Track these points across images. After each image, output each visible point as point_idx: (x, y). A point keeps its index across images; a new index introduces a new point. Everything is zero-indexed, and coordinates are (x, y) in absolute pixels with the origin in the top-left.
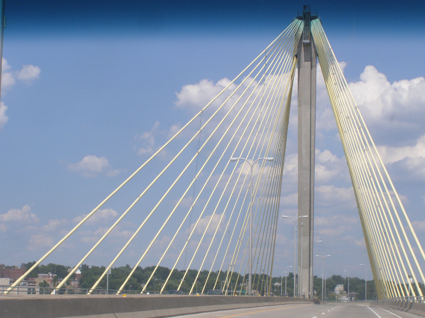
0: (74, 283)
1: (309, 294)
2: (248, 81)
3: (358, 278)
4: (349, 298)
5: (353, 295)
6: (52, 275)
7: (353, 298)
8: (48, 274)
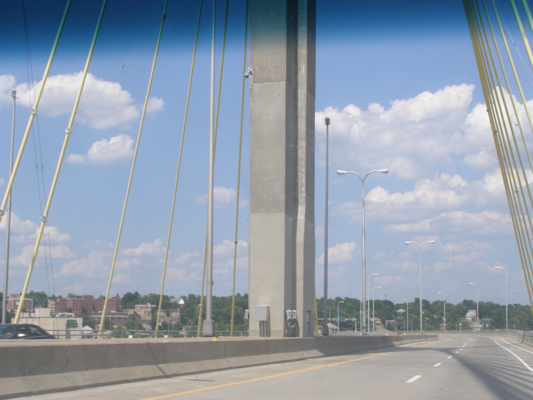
0: (176, 315)
1: (286, 317)
2: (375, 107)
3: (492, 303)
4: (482, 325)
5: (487, 321)
6: (151, 306)
7: (487, 325)
8: (147, 304)
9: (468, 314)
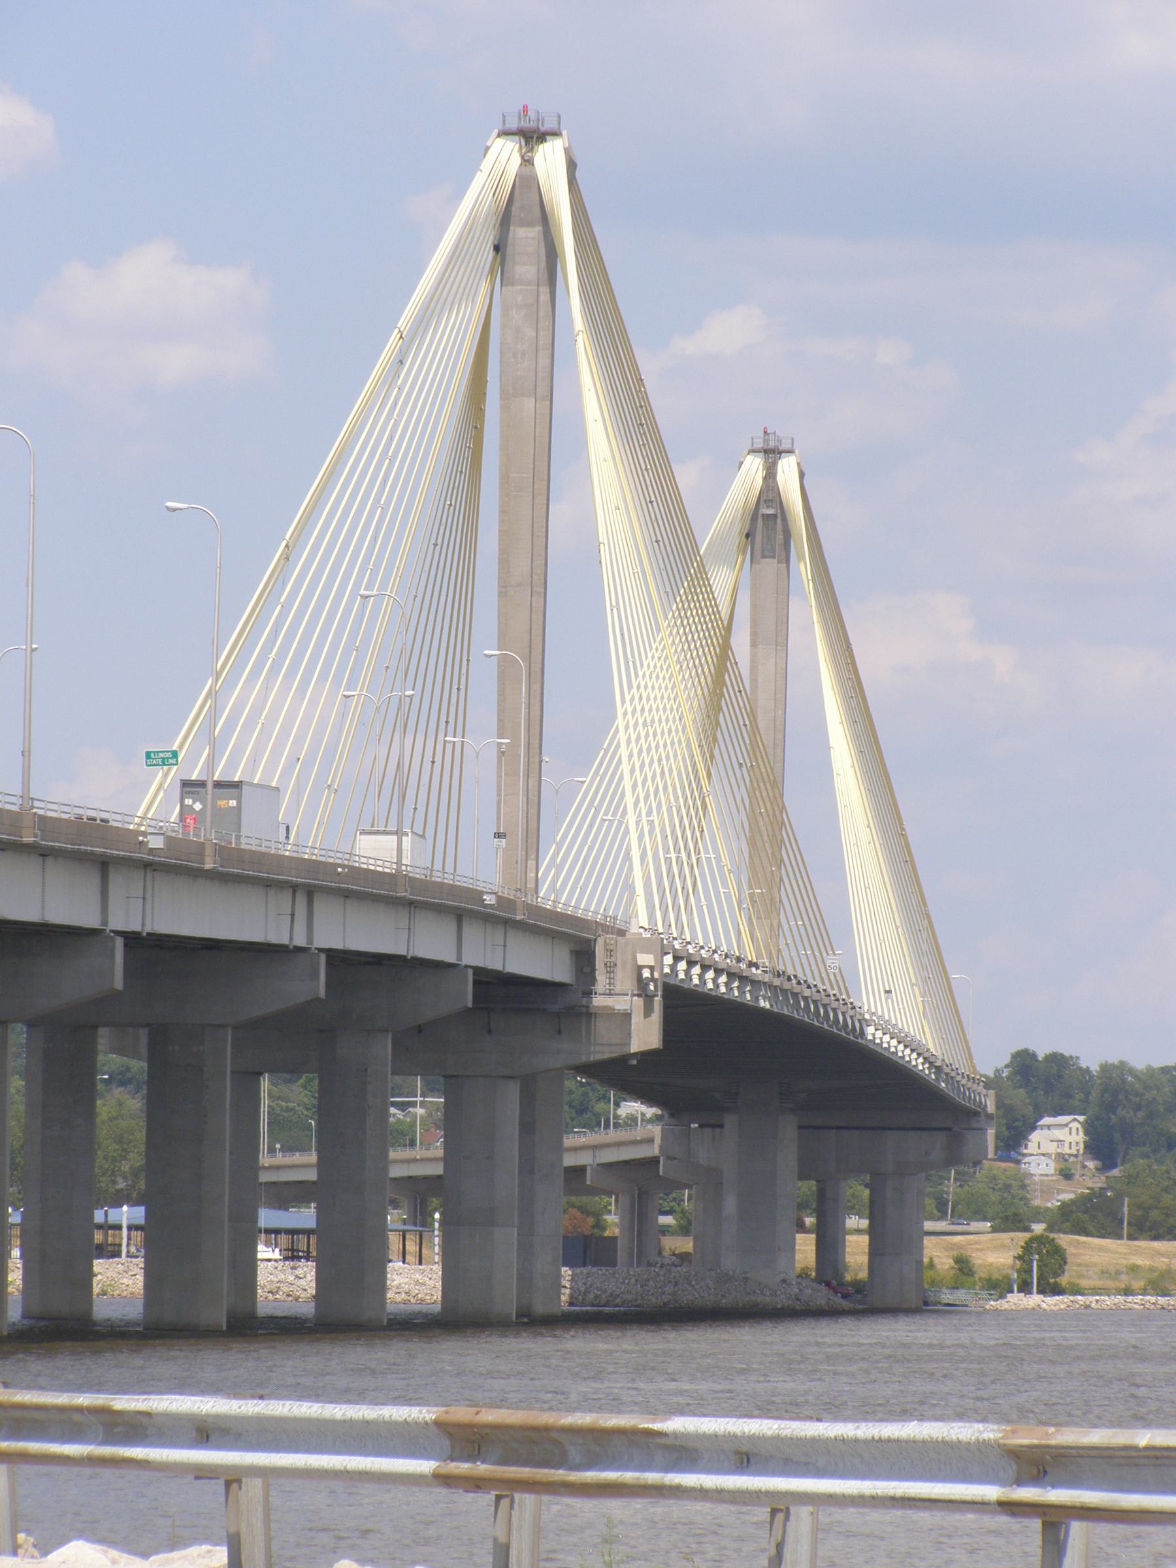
9: (1035, 1137)
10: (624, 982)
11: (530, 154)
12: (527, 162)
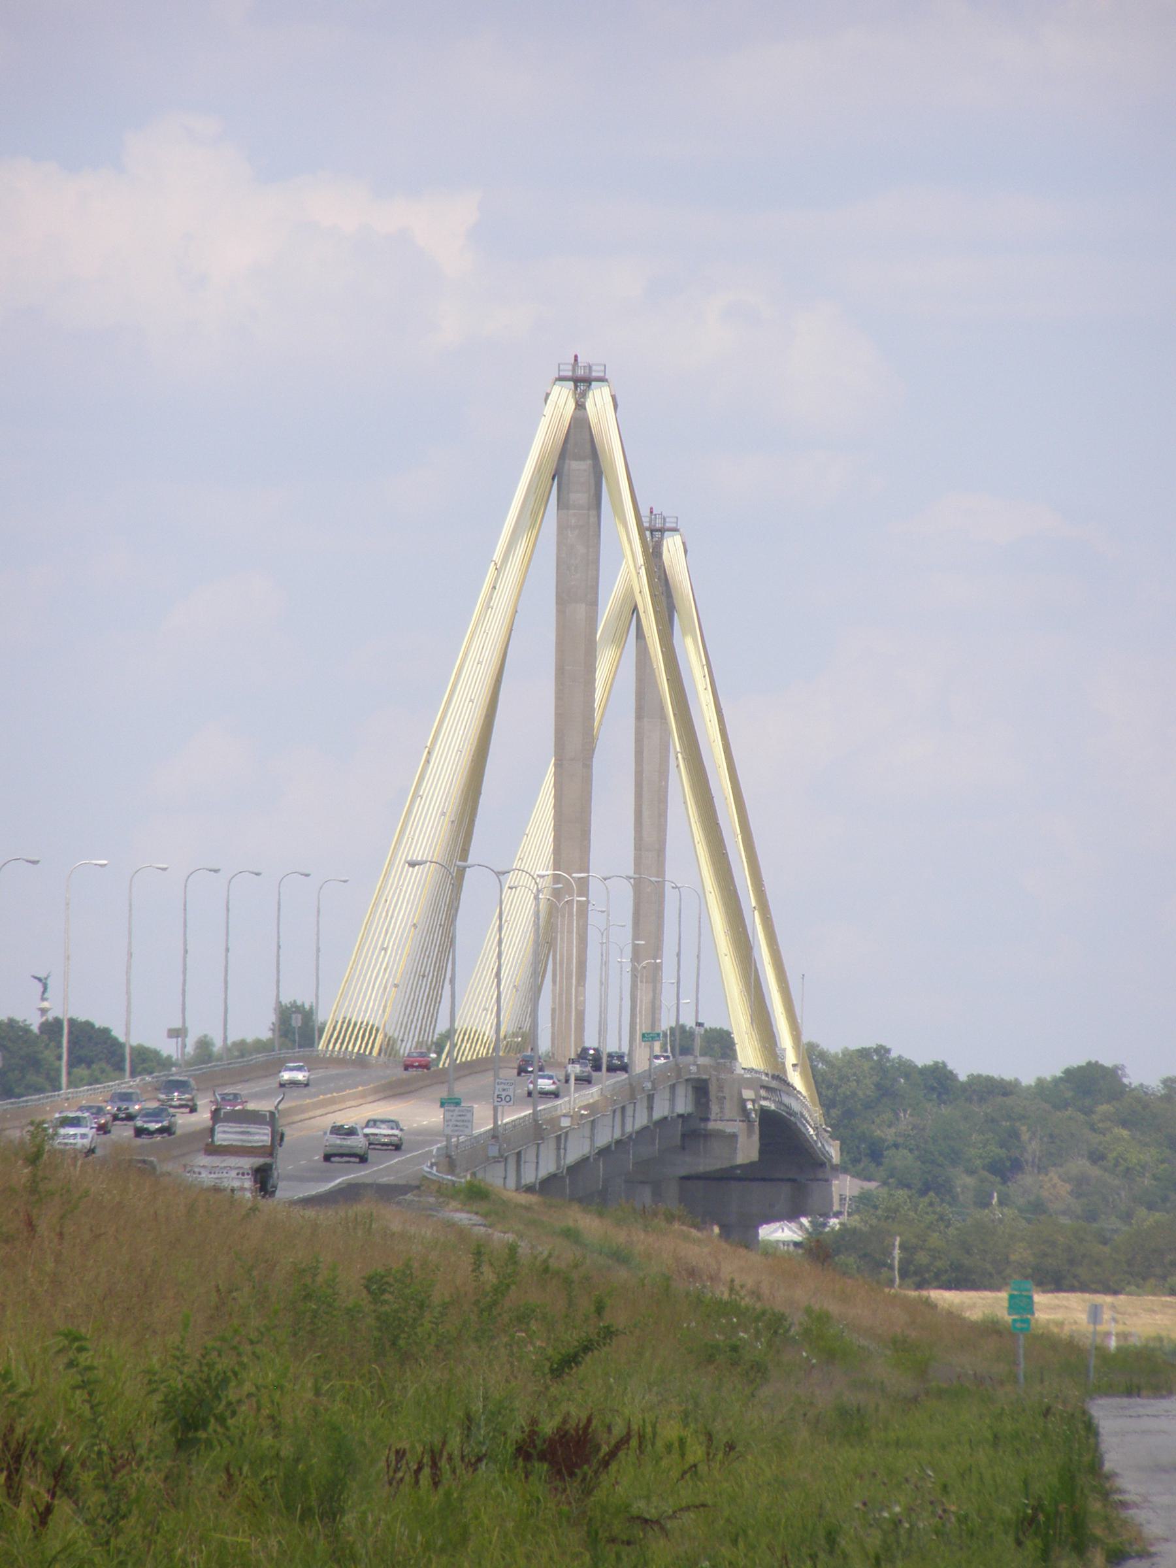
3: (894, 1055)
10: (730, 1110)
11: (582, 400)
12: (580, 406)
